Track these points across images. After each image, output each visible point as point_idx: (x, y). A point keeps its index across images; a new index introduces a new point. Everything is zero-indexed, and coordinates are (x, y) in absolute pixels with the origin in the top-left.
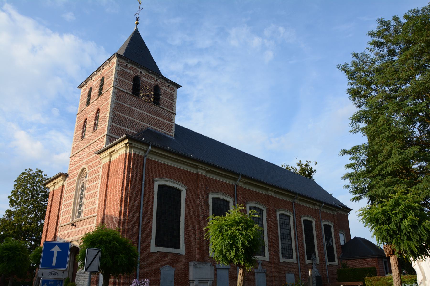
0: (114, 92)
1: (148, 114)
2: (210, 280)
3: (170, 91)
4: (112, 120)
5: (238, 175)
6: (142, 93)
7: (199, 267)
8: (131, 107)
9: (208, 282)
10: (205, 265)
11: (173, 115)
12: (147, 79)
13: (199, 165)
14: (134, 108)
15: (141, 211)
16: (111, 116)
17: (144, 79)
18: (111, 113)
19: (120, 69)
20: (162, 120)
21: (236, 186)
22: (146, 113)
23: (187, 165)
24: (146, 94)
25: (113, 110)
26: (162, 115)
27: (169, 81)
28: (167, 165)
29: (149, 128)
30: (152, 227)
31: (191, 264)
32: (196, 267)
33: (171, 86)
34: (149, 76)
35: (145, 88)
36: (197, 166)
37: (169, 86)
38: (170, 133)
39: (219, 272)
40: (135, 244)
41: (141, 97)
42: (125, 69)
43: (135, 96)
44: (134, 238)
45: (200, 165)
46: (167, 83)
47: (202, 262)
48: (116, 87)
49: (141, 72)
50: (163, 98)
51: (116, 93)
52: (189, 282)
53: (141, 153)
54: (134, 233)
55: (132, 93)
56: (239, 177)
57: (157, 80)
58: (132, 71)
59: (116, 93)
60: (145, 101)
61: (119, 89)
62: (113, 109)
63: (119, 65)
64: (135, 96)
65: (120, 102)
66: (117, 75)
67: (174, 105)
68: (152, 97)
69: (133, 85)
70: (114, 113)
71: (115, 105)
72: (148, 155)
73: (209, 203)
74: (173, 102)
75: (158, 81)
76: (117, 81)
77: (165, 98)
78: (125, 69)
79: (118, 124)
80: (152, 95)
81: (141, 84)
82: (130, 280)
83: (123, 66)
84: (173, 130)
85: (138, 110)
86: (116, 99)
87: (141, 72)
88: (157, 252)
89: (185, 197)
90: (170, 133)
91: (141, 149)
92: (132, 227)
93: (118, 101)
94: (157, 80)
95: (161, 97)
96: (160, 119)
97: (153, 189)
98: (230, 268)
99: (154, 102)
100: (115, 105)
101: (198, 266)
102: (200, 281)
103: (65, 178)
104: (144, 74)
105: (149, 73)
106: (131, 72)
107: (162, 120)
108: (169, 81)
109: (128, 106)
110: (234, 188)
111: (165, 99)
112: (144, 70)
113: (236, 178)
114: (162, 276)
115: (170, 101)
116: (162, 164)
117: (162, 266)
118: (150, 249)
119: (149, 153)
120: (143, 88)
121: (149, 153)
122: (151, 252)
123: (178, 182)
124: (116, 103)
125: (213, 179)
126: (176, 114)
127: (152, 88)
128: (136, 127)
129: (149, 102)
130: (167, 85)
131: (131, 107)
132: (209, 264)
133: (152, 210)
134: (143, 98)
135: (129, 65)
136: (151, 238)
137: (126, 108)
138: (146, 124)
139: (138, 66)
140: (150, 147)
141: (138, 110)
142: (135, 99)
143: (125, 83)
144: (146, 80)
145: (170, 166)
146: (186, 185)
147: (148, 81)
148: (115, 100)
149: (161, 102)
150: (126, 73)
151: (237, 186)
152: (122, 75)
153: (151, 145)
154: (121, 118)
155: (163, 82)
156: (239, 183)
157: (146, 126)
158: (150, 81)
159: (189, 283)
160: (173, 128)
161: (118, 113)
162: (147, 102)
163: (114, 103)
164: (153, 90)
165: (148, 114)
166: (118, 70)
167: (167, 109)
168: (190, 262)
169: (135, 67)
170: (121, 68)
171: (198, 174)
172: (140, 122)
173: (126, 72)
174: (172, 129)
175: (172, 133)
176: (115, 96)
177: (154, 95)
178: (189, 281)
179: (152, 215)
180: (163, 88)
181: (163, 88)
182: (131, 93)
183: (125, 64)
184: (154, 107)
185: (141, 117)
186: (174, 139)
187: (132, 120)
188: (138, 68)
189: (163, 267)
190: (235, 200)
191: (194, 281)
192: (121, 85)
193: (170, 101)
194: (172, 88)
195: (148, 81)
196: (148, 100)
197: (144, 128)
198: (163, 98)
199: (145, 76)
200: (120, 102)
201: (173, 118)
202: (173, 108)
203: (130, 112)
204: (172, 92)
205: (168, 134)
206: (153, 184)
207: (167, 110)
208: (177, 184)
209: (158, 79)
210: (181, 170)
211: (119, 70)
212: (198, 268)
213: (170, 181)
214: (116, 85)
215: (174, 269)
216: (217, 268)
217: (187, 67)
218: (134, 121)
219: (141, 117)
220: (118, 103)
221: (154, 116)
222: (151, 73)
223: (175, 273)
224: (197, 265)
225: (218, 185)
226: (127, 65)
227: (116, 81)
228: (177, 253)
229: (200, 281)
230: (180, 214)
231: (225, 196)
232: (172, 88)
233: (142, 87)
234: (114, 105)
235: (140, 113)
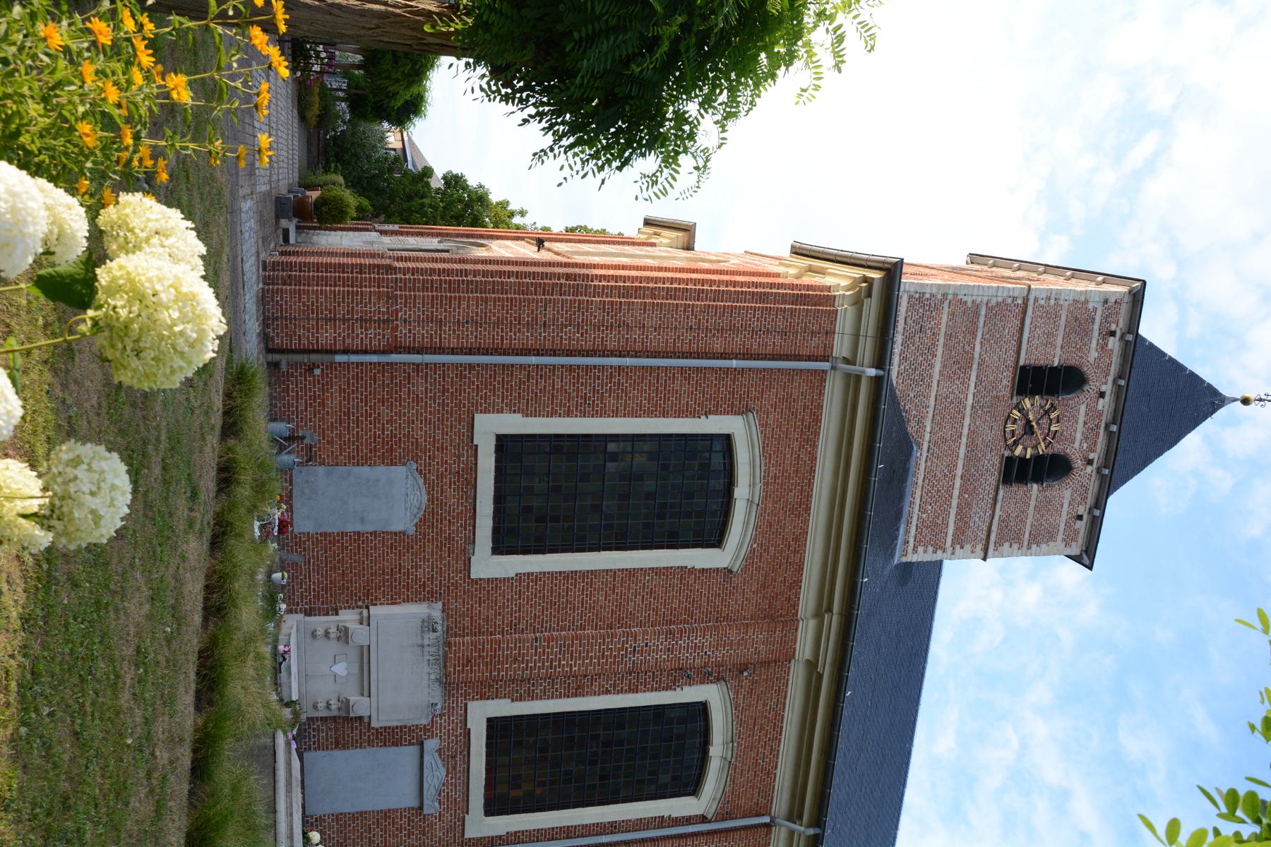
0: (1011, 294)
1: (964, 440)
2: (374, 705)
3: (1062, 526)
4: (917, 296)
5: (818, 820)
6: (1032, 405)
7: (422, 646)
8: (975, 366)
9: (362, 695)
10: (433, 677)
11: (979, 547)
12: (1085, 423)
13: (835, 618)
14: (973, 378)
15: (628, 361)
16: (928, 291)
17: (1083, 409)
18: (940, 292)
19: (1095, 309)
20: (955, 502)
21: (766, 820)
22: (965, 431)
23: (824, 565)
24: (1031, 422)
25: (950, 297)
26: (972, 500)
27: (1097, 513)
28: (812, 471)
29: (915, 448)
30: (568, 416)
31: (435, 611)
32: (423, 632)
33: (1081, 526)
34: (1098, 426)
35: (1053, 416)
36: (830, 610)
37: (1080, 518)
38: (911, 540)
39: (407, 754)
40: (502, 340)
41: (1018, 404)
42: (1096, 327)
43: (1015, 375)
44: (523, 334)
45: (834, 621)
46: (1088, 506)
47: (445, 667)
48: (1032, 298)
49: (1102, 395)
50: (1033, 498)
51: (1009, 301)
52: (361, 607)
53: (841, 347)
54: (540, 333)
55: (1023, 368)
56: (809, 826)
57: (1090, 462)
58: (1099, 358)
59: (1009, 301)
60: (1006, 423)
61: (1024, 312)
62: (955, 295)
63: (1106, 302)
64: (1015, 375)
65: (982, 320)
66: (1071, 299)
67: (1016, 546)
68: (1025, 449)
69: (1053, 369)
70: (942, 302)
71: (969, 304)
72: (837, 372)
73: (686, 688)
74: (1026, 543)
75: (1089, 469)
76: (1052, 302)
77: (1033, 503)
78: (1096, 327)
79: (909, 321)
80: (1035, 447)
81: (1063, 399)
82: (366, 320)
83: (1106, 319)
84: (925, 552)
85: (970, 397)
86: (990, 305)
87: (1102, 395)
88: (475, 443)
89: (698, 566)
90: (911, 540)
91: (856, 335)
92: (562, 324)
93: (983, 312)
94: (1090, 462)
95: (1035, 486)
96: (956, 493)
97: (716, 413)
98: (426, 811)
99: (1009, 461)
100: (969, 304)
101: (426, 642)
102: (365, 649)
103: (680, 245)
104: (1100, 407)
105: (1107, 426)
106: (1093, 354)
107: (955, 502)
108: (1097, 513)
109: (976, 355)
110: (758, 815)
111: (1032, 508)
112: (1113, 405)
113: (800, 817)
114: (381, 472)
115: (1028, 528)
116: (814, 446)
117: (421, 473)
118: (486, 411)
119: (848, 376)
120: (1049, 409)
121: (848, 376)
122: (473, 419)
123: (756, 527)
124: (976, 307)
125: (784, 704)
126: (984, 559)
127: (1058, 448)
128: (912, 395)
129: (1006, 440)
130: (1082, 510)
131: (975, 366)
132: (437, 695)
133: (633, 414)
134: (1014, 411)
135: (1117, 344)
136: (527, 416)
137: (967, 348)
138: (927, 437)
139: (1120, 376)
140: (872, 372)
141: (970, 397)
142: (1006, 381)
143: (1050, 335)
144: (1081, 419)
145: (810, 484)
146: (745, 569)
147: (1080, 426)
148: (985, 300)
149: (1018, 490)
150: (1085, 335)
151: (768, 826)
152: (1076, 319)
153: (881, 373)
154: (928, 331)
155: (1087, 489)
156: (783, 829)
157: (922, 437)
158: (1079, 436)
159: (360, 603)
160: (935, 552)
161: (945, 317)
162: (1005, 431)
163: (974, 298)
164: (1050, 451)
165: (964, 440)
166: (1087, 301)
167: (997, 517)
168: (444, 604)
169: (1113, 368)
170: (1099, 313)
171: (798, 621)
172: (931, 410)
173: (1087, 333)
174: (930, 549)
175: (915, 550)
176: (1000, 300)
177: (1038, 458)
178: (367, 608)
179: (616, 414)
180: (1067, 494)
181: (1067, 494)
182: (1021, 363)
183: (1113, 327)
184: (992, 464)
185: (949, 411)
186: (896, 562)
187: (931, 376)
188: (1115, 381)
189: (417, 474)
190: (710, 822)
191: (365, 622)
192: (1041, 317)
193: (1028, 528)
194: (1077, 532)
195: (1080, 426)
196: (1013, 432)
197: (912, 428)
198: (1033, 498)
199: (1093, 413)
200: (982, 320)
201: (968, 547)
202: (1007, 545)
203: (959, 364)
204: (1060, 536)
205: (907, 532)
206: (732, 410)
207: (993, 517)
208: (746, 523)
209: (1095, 465)
210: (800, 539)
211: (1090, 306)
212: (420, 642)
213: (754, 484)
214: (1036, 300)
215: (411, 531)
216: (421, 744)
217: (1061, 798)
218: (929, 386)
219: (949, 411)
220: (977, 314)
221: (960, 463)
222: (1110, 434)
223: (396, 534)
224: (432, 635)
225: (762, 728)
226: (1113, 334)
227: (1049, 298)
228: (474, 542)
229: (365, 649)
230: (587, 806)
231: (721, 769)
232: (1077, 532)
233: (1052, 405)
234: (969, 299)
235: (961, 403)
